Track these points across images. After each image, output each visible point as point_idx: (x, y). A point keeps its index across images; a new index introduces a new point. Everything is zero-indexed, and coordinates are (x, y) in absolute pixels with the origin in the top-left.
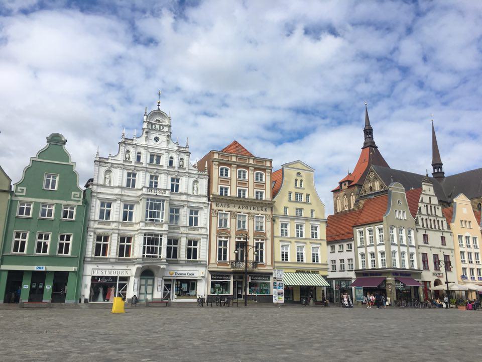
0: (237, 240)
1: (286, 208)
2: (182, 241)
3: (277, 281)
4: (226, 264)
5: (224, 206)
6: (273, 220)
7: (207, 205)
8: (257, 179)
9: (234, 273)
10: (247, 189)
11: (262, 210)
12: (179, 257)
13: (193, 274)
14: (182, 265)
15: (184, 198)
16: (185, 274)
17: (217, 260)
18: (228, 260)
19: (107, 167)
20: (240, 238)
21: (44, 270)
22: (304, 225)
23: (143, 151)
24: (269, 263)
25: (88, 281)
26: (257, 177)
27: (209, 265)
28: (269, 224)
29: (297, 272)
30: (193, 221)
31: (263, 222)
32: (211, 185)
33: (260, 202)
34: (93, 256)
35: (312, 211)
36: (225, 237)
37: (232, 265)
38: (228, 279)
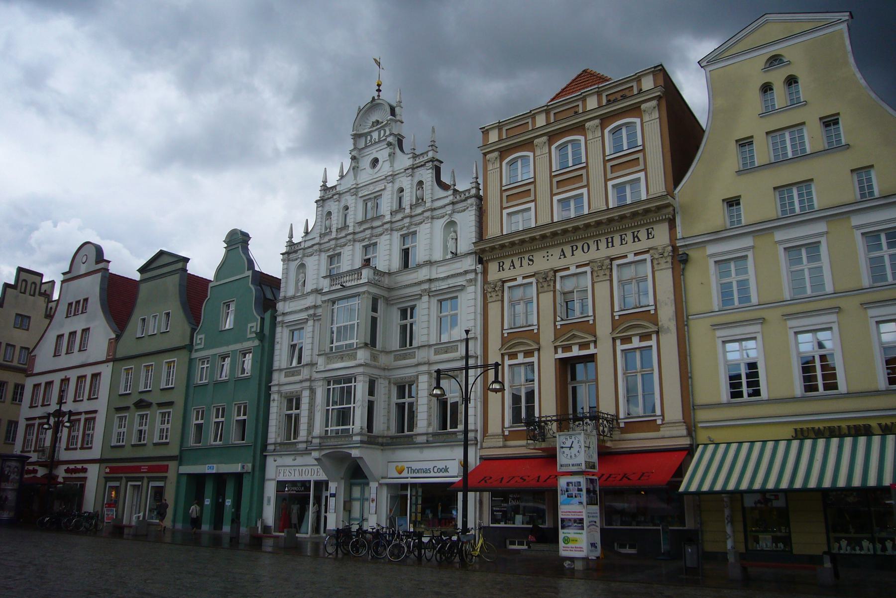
0: (561, 355)
1: (733, 202)
5: (517, 263)
6: (680, 260)
10: (642, 175)
13: (446, 470)
14: (428, 445)
16: (426, 471)
19: (447, 217)
21: (214, 471)
22: (823, 240)
23: (349, 200)
25: (270, 490)
28: (666, 278)
29: (801, 435)
31: (645, 279)
32: (484, 218)
35: (862, 171)
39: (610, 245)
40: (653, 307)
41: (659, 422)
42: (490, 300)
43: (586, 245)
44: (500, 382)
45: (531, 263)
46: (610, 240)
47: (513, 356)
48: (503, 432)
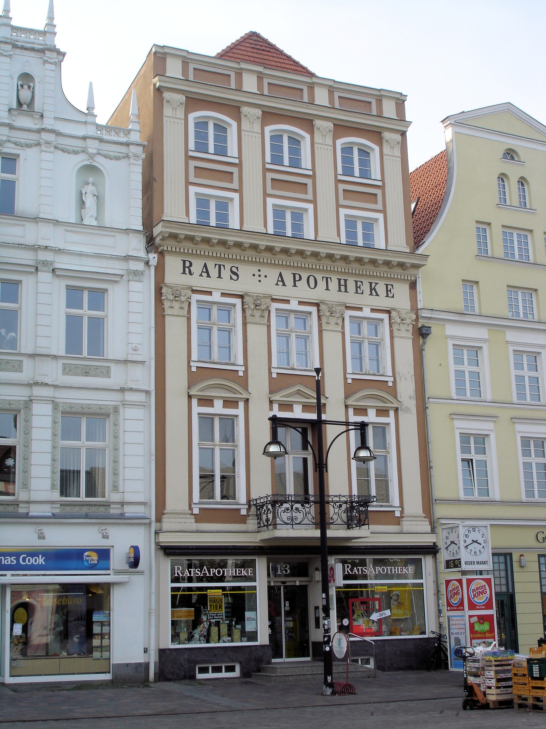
2: (36, 421)
3: (464, 573)
4: (233, 516)
7: (140, 266)
8: (348, 171)
9: (274, 551)
11: (373, 290)
12: (26, 486)
15: (31, 234)
17: (196, 497)
18: (242, 497)
20: (288, 406)
24: (414, 504)
26: (277, 148)
27: (159, 520)
30: (85, 338)
33: (294, 246)
34: (56, 495)
36: (230, 403)
37: (259, 517)
38: (178, 589)
39: (343, 288)
40: (243, 368)
41: (398, 514)
42: (168, 311)
43: (312, 279)
44: (279, 443)
45: (235, 277)
46: (342, 282)
47: (207, 401)
48: (191, 508)
